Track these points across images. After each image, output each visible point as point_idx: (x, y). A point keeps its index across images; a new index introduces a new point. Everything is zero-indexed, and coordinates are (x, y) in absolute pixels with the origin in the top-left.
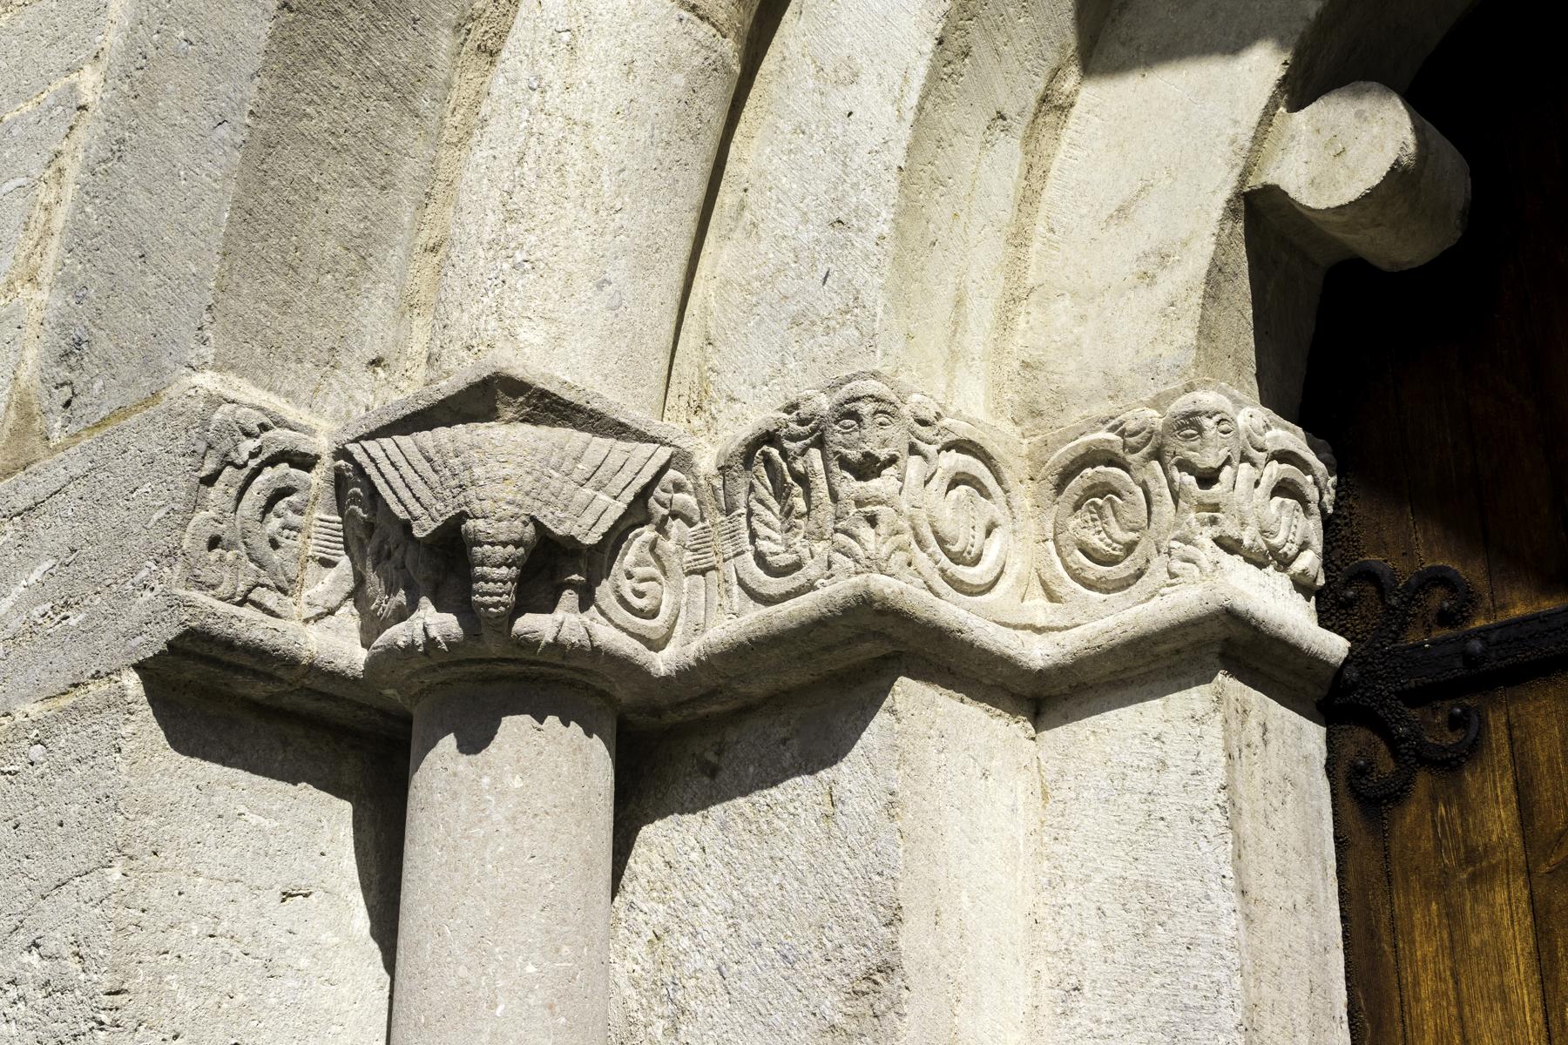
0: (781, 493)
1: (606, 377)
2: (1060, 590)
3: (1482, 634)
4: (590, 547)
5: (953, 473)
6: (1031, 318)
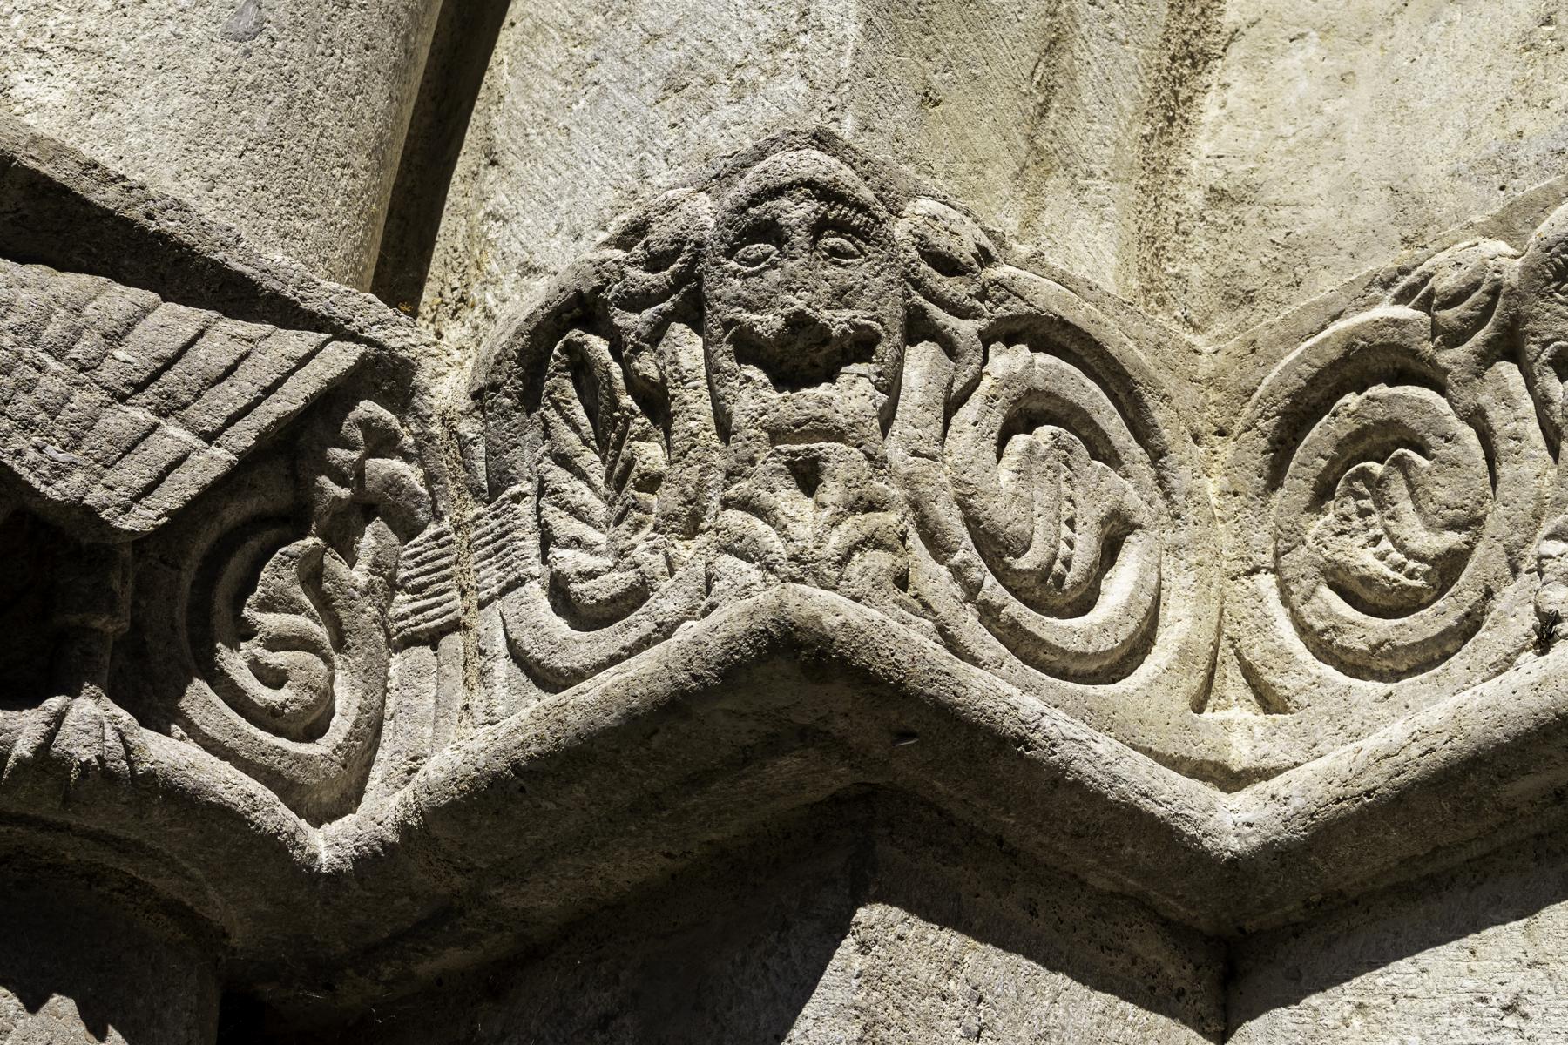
0: (608, 433)
1: (213, 183)
2: (1285, 683)
4: (139, 541)
5: (1018, 388)
6: (1229, 95)
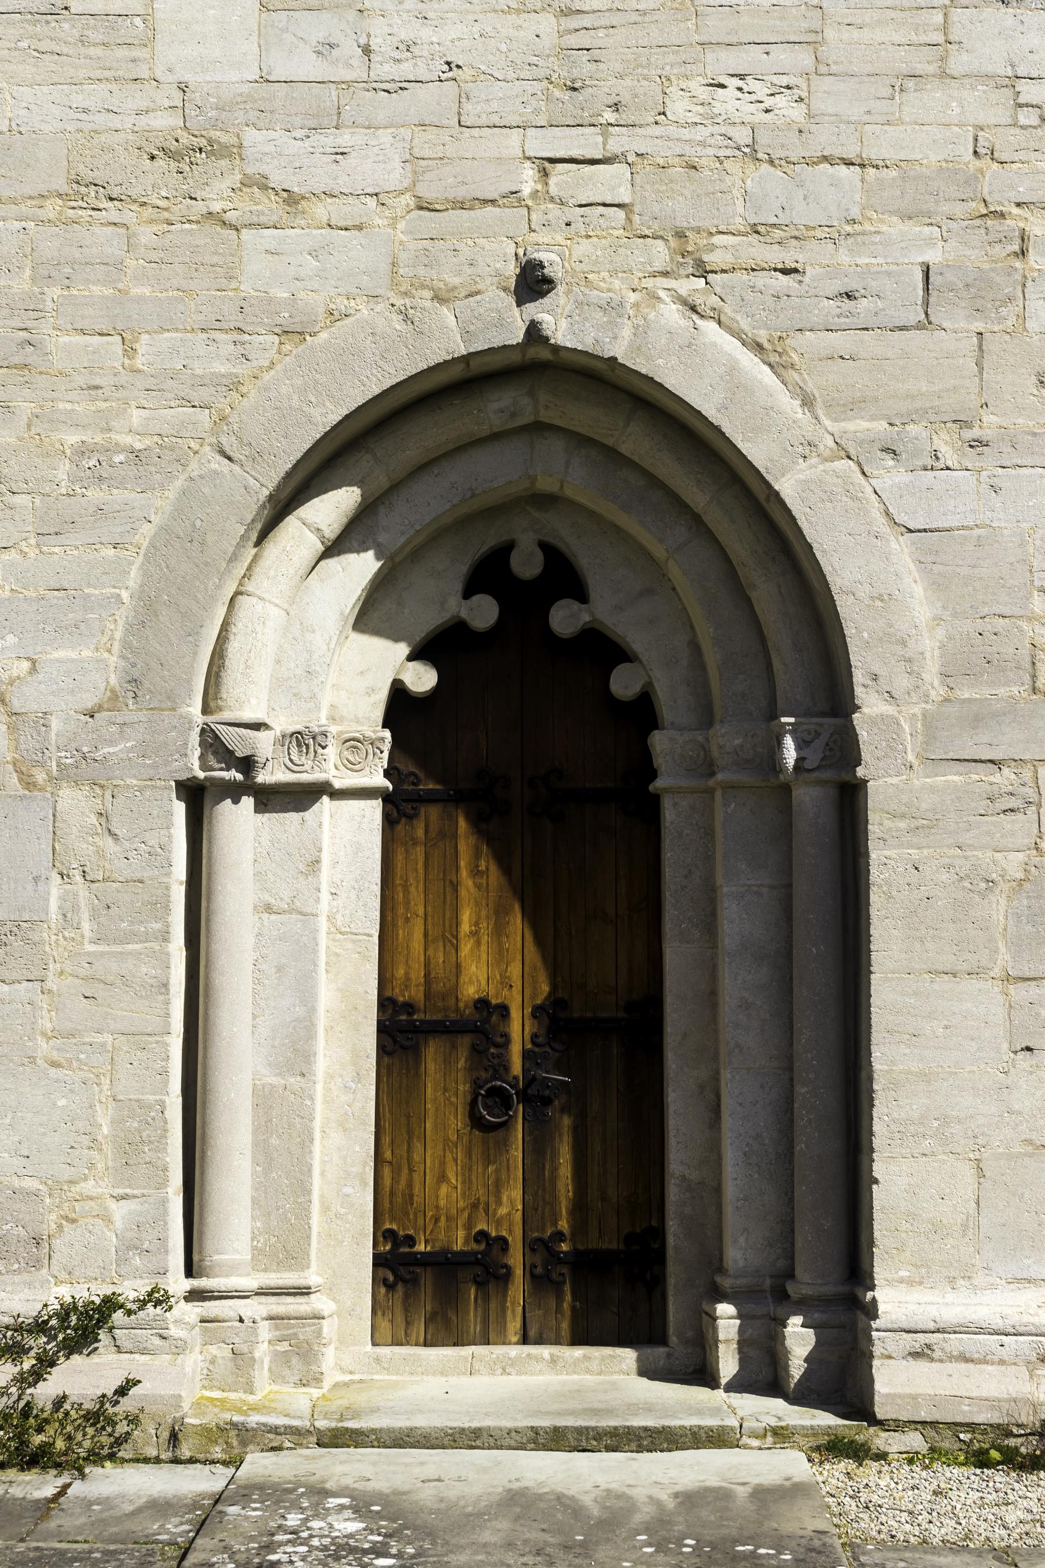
3: (423, 790)
